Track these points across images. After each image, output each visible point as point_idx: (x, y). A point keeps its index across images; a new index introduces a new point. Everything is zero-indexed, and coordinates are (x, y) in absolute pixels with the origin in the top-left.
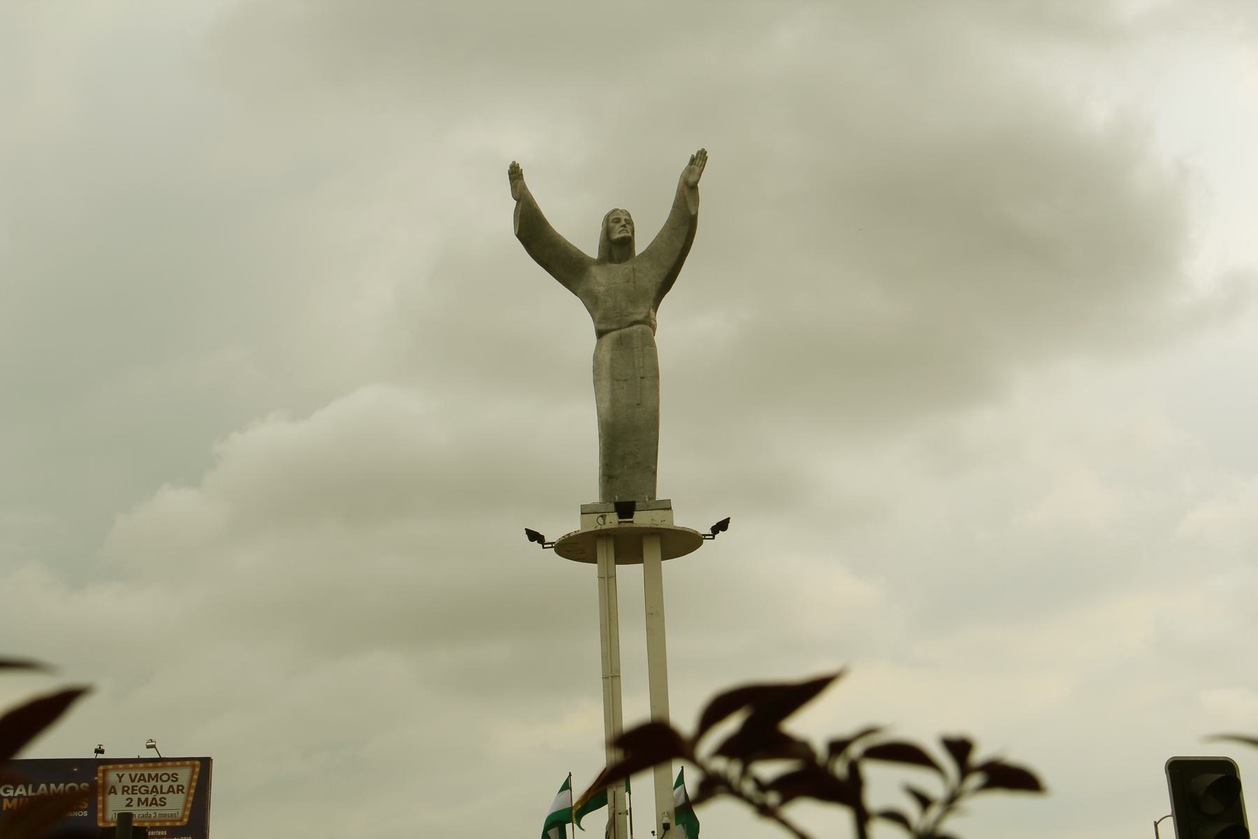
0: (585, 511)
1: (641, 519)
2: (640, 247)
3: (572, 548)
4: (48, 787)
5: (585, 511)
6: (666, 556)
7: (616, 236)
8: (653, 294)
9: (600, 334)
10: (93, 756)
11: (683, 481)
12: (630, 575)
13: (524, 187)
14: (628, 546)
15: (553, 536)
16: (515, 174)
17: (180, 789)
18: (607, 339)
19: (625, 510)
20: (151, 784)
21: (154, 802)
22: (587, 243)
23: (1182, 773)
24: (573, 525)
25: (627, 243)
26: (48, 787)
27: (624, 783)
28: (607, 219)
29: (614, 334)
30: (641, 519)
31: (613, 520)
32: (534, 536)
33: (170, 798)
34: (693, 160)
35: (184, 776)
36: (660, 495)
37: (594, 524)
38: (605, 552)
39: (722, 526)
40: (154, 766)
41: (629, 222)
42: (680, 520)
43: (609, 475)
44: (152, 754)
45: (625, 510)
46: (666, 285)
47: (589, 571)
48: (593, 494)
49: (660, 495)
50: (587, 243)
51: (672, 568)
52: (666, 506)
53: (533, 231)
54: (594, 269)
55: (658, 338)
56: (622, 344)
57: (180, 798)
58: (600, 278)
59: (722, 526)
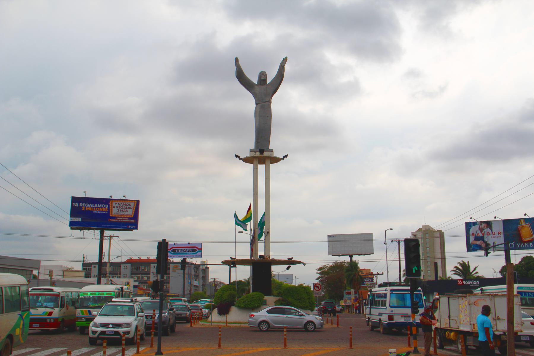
0: (251, 151)
1: (266, 154)
2: (268, 81)
3: (247, 160)
4: (79, 205)
5: (251, 151)
6: (271, 163)
7: (262, 78)
8: (271, 94)
9: (257, 104)
10: (109, 198)
11: (276, 144)
12: (261, 168)
13: (239, 64)
14: (262, 160)
15: (242, 157)
16: (237, 60)
17: (131, 208)
18: (258, 105)
19: (262, 151)
20: (124, 206)
21: (124, 211)
22: (255, 81)
23: (407, 241)
24: (247, 154)
25: (265, 80)
26: (79, 205)
27: (98, 232)
28: (260, 73)
29: (261, 104)
30: (266, 154)
31: (258, 154)
32: (237, 156)
33: (129, 210)
34: (284, 60)
35: (132, 205)
36: (270, 148)
37: (253, 154)
38: (256, 161)
39: (286, 156)
40: (124, 202)
41: (266, 75)
42: (276, 154)
43: (257, 142)
44: (124, 198)
45: (262, 151)
46: (275, 92)
47: (251, 166)
48: (253, 147)
49: (270, 148)
50: (255, 81)
51: (272, 166)
52: (272, 151)
53: (241, 77)
54: (257, 87)
55: (272, 106)
56: (262, 107)
57: (131, 210)
58: (257, 90)
59: (286, 156)
